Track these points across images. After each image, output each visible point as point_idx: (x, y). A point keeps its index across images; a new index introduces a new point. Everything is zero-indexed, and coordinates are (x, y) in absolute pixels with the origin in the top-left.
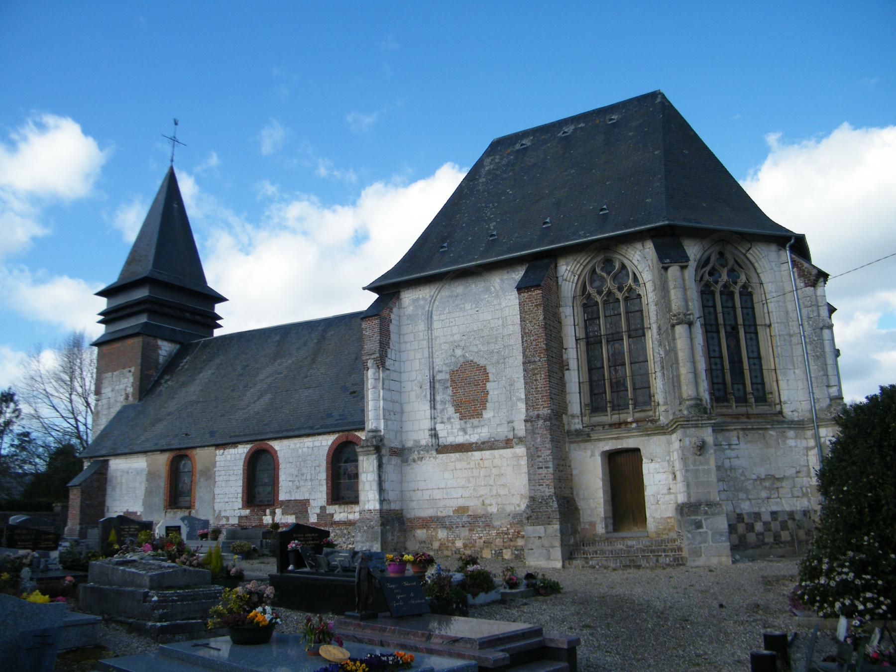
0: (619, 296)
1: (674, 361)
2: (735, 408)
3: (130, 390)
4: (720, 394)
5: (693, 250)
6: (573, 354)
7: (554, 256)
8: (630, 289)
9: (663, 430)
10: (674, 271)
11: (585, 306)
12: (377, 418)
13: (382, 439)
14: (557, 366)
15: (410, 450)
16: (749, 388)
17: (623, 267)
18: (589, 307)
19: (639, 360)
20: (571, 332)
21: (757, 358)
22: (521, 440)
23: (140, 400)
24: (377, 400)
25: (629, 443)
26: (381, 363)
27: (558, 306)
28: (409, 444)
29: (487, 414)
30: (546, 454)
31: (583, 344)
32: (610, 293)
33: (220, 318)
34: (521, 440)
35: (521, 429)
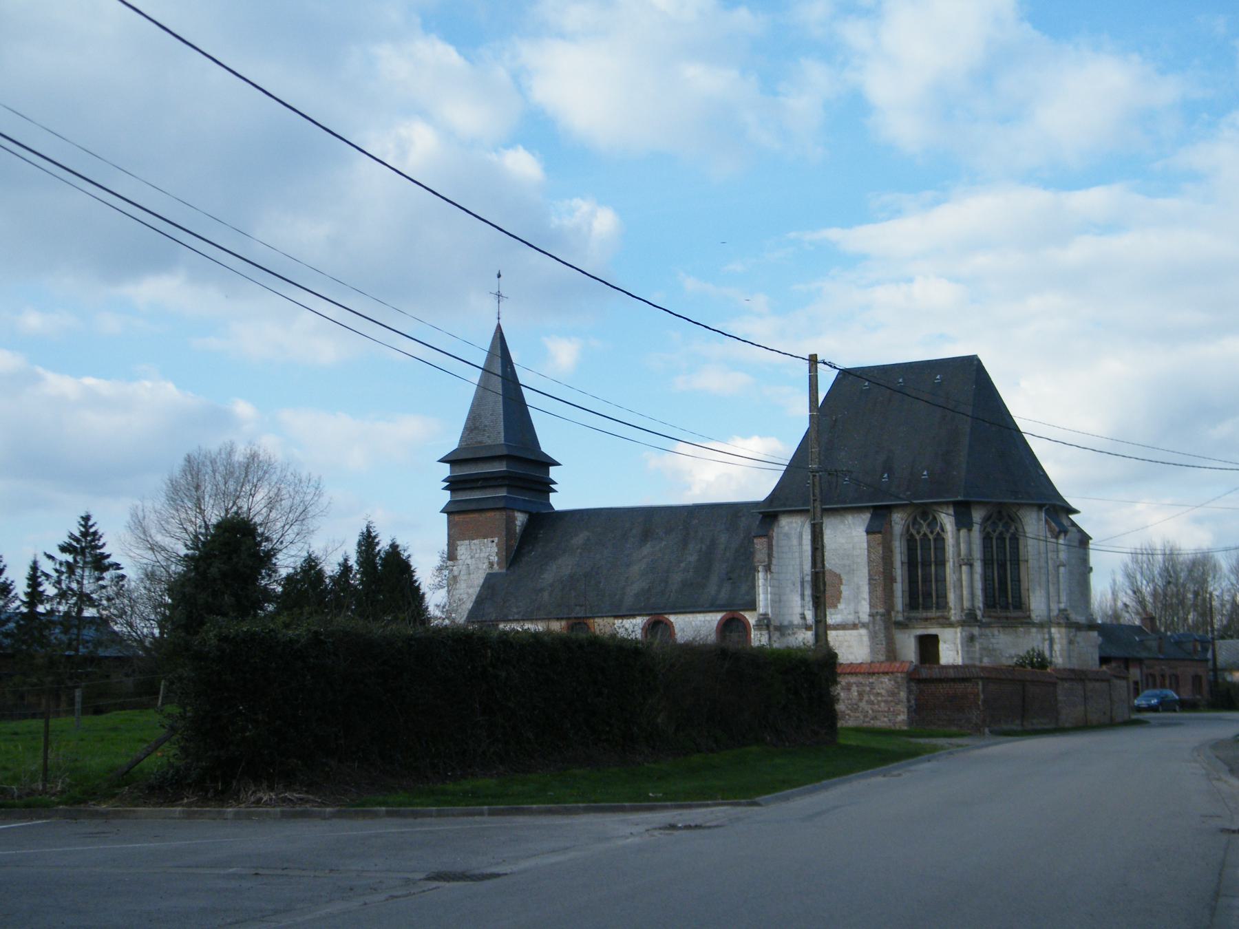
0: (931, 537)
1: (963, 584)
2: (999, 613)
3: (495, 559)
4: (990, 603)
5: (977, 516)
6: (899, 572)
7: (889, 509)
8: (938, 534)
9: (951, 625)
10: (963, 532)
11: (908, 541)
12: (766, 606)
13: (769, 620)
14: (889, 579)
15: (787, 627)
16: (1010, 600)
17: (935, 518)
18: (911, 542)
19: (941, 580)
20: (899, 557)
21: (1017, 581)
22: (864, 625)
23: (508, 569)
24: (766, 593)
25: (932, 631)
26: (768, 568)
27: (891, 541)
28: (786, 623)
29: (840, 606)
30: (881, 636)
31: (906, 567)
32: (925, 534)
33: (554, 483)
34: (864, 625)
35: (865, 618)
